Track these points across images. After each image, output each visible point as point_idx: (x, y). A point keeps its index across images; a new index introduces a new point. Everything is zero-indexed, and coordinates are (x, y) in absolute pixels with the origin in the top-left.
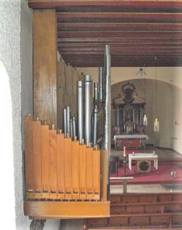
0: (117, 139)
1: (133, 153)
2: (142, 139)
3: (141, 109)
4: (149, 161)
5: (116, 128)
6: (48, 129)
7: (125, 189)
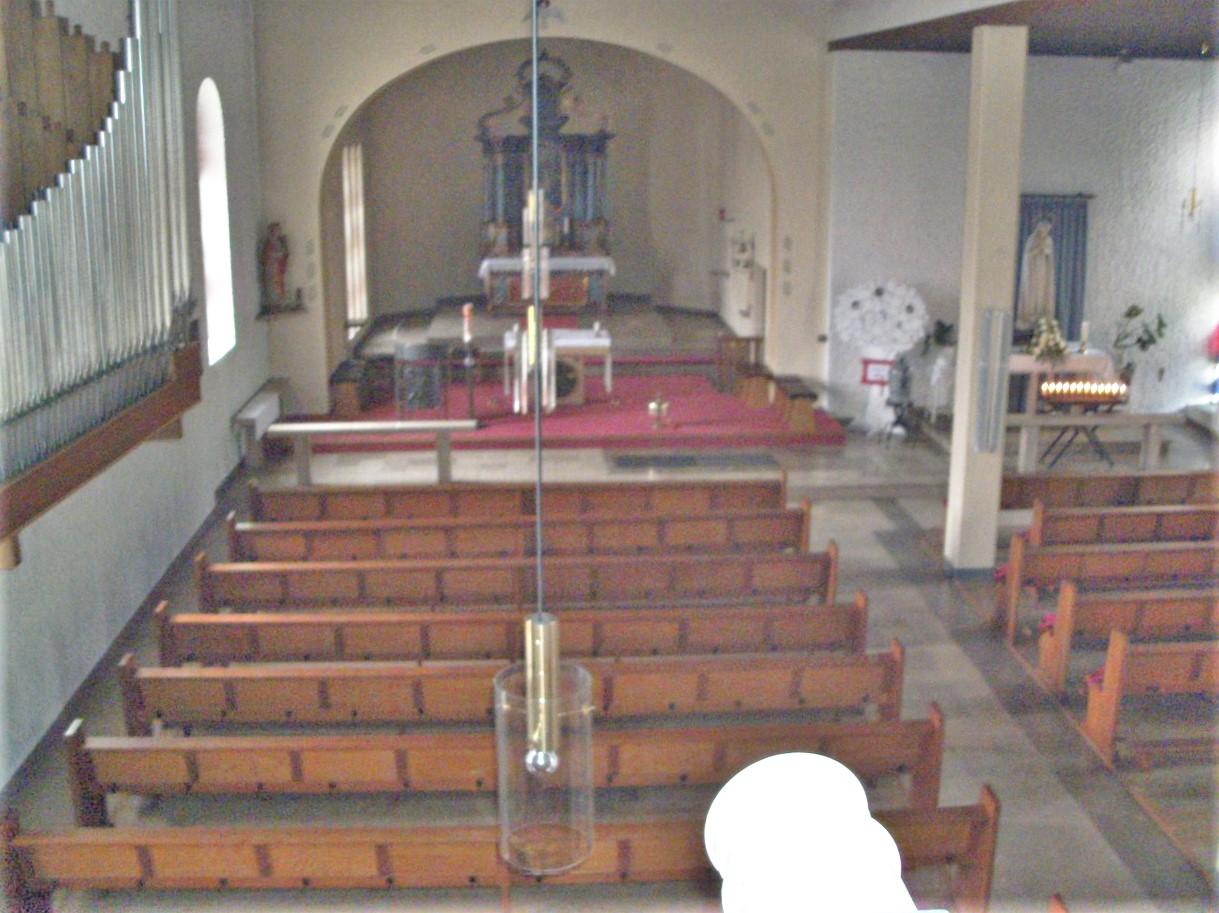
0: (494, 274)
1: (597, 326)
2: (590, 273)
3: (590, 159)
4: (577, 358)
5: (492, 230)
6: (570, 121)
7: (444, 467)
